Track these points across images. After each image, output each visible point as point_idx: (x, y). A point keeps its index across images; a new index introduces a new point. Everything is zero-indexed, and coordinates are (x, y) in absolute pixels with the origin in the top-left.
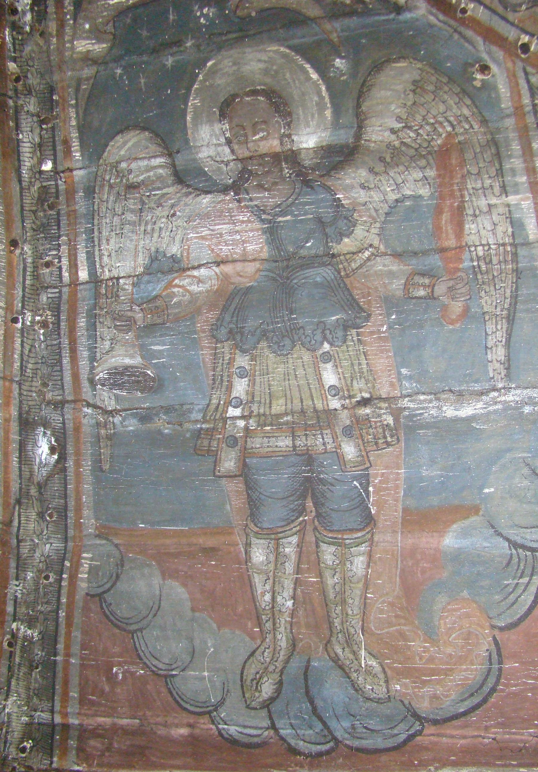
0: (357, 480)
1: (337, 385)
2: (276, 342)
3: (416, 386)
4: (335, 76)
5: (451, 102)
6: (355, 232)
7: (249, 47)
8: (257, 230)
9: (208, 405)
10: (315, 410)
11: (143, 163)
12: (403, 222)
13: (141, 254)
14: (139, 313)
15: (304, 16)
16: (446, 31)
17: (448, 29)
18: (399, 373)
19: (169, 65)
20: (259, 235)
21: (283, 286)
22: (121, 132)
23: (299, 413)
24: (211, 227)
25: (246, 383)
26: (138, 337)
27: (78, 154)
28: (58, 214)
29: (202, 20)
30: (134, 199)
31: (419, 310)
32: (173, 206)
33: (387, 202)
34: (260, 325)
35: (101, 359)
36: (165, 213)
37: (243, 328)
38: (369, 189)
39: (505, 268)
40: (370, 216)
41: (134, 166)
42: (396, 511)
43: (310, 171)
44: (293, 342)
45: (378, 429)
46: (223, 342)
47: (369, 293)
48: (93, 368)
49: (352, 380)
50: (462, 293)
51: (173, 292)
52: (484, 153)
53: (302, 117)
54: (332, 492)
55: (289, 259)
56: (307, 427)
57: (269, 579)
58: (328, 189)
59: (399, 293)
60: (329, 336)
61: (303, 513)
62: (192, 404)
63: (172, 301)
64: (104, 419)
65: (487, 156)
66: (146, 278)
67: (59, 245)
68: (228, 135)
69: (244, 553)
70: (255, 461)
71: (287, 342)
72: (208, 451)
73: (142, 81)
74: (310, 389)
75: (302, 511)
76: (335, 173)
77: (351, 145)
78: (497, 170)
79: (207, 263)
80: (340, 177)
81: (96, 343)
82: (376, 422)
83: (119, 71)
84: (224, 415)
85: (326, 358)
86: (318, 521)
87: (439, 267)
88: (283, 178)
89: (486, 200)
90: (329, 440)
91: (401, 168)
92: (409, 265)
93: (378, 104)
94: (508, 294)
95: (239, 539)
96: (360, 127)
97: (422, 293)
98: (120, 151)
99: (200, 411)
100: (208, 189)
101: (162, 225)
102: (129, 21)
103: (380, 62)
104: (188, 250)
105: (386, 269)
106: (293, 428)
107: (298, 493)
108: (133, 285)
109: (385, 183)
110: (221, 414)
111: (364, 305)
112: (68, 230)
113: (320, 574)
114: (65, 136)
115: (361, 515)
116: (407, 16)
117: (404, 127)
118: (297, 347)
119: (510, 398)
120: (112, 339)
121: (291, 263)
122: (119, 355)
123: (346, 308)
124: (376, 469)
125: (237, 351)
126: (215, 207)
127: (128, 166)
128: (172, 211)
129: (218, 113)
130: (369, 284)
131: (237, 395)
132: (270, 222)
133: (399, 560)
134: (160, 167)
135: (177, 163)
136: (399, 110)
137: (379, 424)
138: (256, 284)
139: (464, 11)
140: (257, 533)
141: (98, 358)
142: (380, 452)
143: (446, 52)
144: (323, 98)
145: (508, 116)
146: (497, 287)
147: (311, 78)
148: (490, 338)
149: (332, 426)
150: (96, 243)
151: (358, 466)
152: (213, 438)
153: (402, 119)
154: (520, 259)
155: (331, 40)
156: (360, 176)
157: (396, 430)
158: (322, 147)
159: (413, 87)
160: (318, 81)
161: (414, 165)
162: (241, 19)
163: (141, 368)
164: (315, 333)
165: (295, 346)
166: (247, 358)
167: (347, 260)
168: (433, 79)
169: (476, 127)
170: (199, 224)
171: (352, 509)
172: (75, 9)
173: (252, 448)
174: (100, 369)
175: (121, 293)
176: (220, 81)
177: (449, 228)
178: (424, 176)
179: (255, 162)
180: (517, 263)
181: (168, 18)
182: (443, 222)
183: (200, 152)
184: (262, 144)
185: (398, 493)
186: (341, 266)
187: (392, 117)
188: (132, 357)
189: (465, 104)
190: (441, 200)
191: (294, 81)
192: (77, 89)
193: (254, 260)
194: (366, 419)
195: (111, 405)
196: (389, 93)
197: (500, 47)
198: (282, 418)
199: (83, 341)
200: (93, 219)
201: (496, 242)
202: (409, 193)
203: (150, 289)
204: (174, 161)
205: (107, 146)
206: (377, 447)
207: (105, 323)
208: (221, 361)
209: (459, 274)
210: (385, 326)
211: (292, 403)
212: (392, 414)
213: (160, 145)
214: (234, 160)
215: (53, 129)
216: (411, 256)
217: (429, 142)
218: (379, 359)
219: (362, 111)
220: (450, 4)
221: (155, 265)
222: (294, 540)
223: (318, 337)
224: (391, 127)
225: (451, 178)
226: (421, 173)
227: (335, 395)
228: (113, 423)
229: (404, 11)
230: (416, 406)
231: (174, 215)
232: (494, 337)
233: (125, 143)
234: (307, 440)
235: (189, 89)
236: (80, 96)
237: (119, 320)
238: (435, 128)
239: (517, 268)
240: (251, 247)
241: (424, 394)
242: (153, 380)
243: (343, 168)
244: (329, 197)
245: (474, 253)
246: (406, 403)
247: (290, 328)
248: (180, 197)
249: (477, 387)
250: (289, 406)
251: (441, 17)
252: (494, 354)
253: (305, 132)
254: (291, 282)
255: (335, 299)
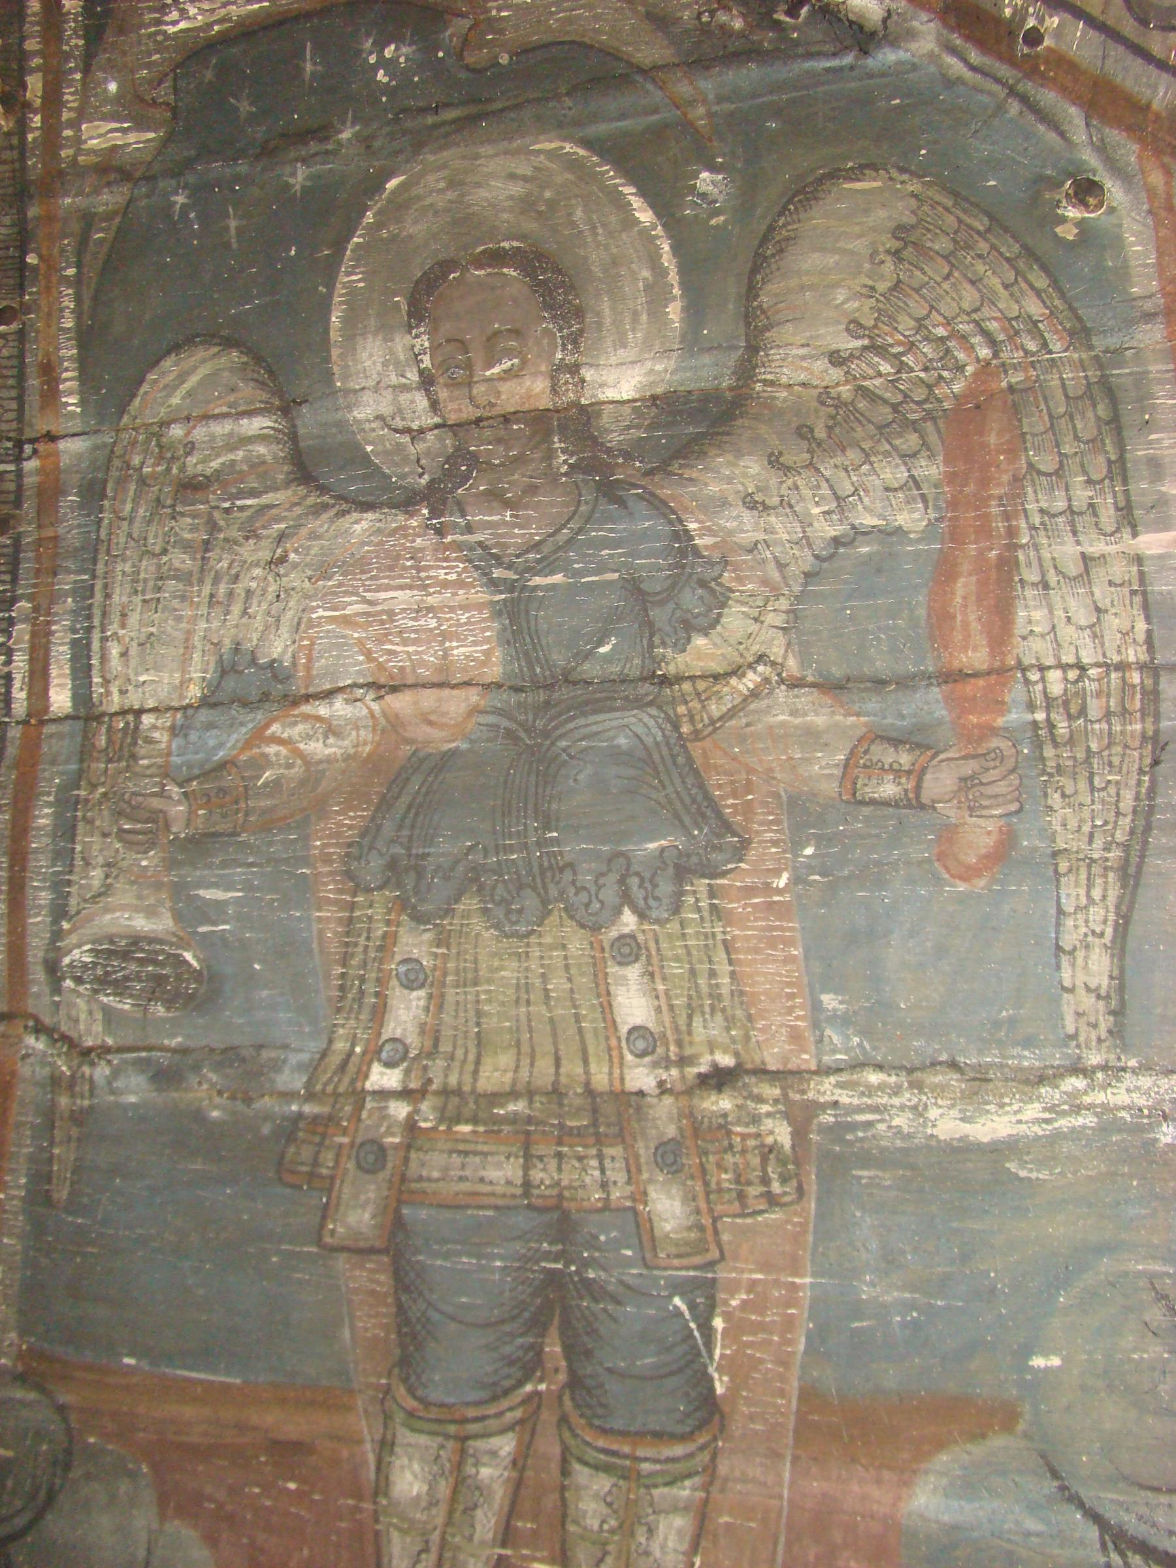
0: (682, 1295)
1: (650, 1025)
2: (503, 900)
3: (860, 1045)
4: (696, 216)
5: (995, 282)
6: (724, 620)
7: (490, 141)
8: (480, 607)
9: (324, 1054)
10: (590, 1092)
11: (221, 429)
12: (850, 597)
13: (197, 656)
14: (179, 802)
15: (630, 64)
16: (990, 93)
17: (996, 88)
18: (817, 1006)
19: (298, 187)
20: (484, 620)
21: (533, 754)
22: (176, 348)
23: (548, 1094)
24: (368, 595)
25: (422, 1003)
26: (171, 864)
27: (72, 400)
28: (17, 544)
29: (381, 76)
30: (194, 517)
31: (878, 836)
32: (281, 537)
33: (810, 545)
34: (467, 854)
35: (78, 913)
36: (265, 555)
37: (425, 856)
38: (766, 508)
39: (1123, 733)
40: (765, 582)
41: (199, 433)
42: (782, 1393)
43: (620, 460)
44: (545, 902)
45: (749, 1156)
46: (369, 890)
47: (749, 782)
48: (58, 935)
49: (690, 1017)
50: (996, 796)
51: (265, 756)
52: (1078, 417)
53: (608, 321)
54: (615, 1320)
55: (552, 685)
56: (565, 1135)
57: (426, 1550)
58: (660, 507)
59: (831, 788)
60: (638, 894)
61: (533, 1371)
62: (286, 1047)
63: (259, 777)
64: (70, 1068)
65: (1086, 426)
66: (204, 715)
67: (11, 622)
68: (426, 362)
69: (373, 1467)
70: (423, 1213)
71: (530, 901)
72: (312, 1176)
73: (233, 224)
74: (580, 1030)
75: (532, 1365)
76: (680, 467)
77: (729, 395)
78: (1109, 462)
79: (355, 685)
80: (694, 475)
81: (70, 872)
82: (744, 1137)
83: (180, 199)
84: (359, 1085)
85: (626, 950)
86: (573, 1399)
87: (940, 722)
88: (552, 477)
89: (1078, 543)
90: (616, 1173)
91: (853, 455)
92: (858, 715)
93: (802, 288)
94: (1127, 802)
95: (367, 1430)
96: (753, 349)
97: (889, 789)
98: (169, 396)
99: (300, 1067)
100: (369, 499)
101: (254, 585)
102: (209, 75)
103: (810, 179)
104: (311, 650)
105: (798, 721)
106: (528, 1133)
107: (527, 1315)
108: (173, 730)
109: (806, 492)
110: (353, 1081)
111: (735, 814)
112: (35, 586)
113: (564, 1552)
114: (47, 355)
115: (687, 1394)
116: (888, 56)
117: (865, 348)
118: (554, 918)
119: (1119, 1096)
120: (108, 865)
121: (556, 695)
122: (123, 908)
123: (687, 820)
124: (735, 1269)
125: (404, 917)
126: (381, 543)
127: (187, 434)
128: (279, 551)
129: (404, 307)
130: (752, 761)
131: (398, 1034)
132: (511, 586)
133: (782, 1539)
134: (261, 438)
135: (302, 431)
136: (856, 305)
137: (751, 1143)
138: (465, 746)
139: (1033, 38)
140: (411, 1414)
141: (73, 911)
142: (749, 1221)
143: (985, 149)
144: (664, 273)
145: (1149, 317)
146: (1097, 782)
147: (638, 222)
148: (1070, 922)
149: (628, 1138)
150: (96, 622)
151: (688, 1255)
152: (327, 1142)
153: (861, 326)
154: (1165, 706)
155: (691, 124)
156: (745, 475)
157: (797, 1163)
158: (654, 398)
159: (895, 244)
160: (655, 229)
161: (888, 447)
162: (474, 71)
163: (171, 944)
164: (601, 881)
165: (550, 912)
166: (427, 936)
167: (698, 694)
168: (950, 220)
169: (1056, 346)
170: (340, 585)
171: (662, 1377)
172: (87, 45)
173: (420, 1179)
174: (73, 939)
175: (142, 749)
176: (415, 228)
177: (972, 617)
178: (912, 477)
179: (488, 433)
180: (1157, 717)
181: (300, 70)
182: (959, 599)
183: (357, 404)
184: (505, 387)
185: (790, 1342)
186: (682, 709)
187: (838, 323)
188: (151, 912)
189: (1032, 287)
190: (953, 541)
191: (594, 228)
192: (83, 241)
193: (467, 684)
194: (720, 1127)
195: (93, 1034)
196: (832, 260)
197: (1130, 129)
198: (502, 1106)
199: (41, 864)
200: (95, 561)
201: (1101, 659)
202: (869, 521)
203: (212, 743)
204: (294, 426)
205: (141, 381)
206: (744, 1205)
207: (98, 823)
208: (362, 940)
209: (995, 743)
210: (785, 876)
211: (532, 1065)
212: (787, 1116)
213: (263, 384)
214: (437, 426)
215: (21, 334)
216: (866, 689)
217: (930, 387)
218: (765, 962)
219: (760, 307)
220: (998, 21)
221: (230, 684)
222: (506, 1445)
223: (610, 894)
224: (834, 347)
225: (985, 483)
226: (903, 468)
227: (641, 1055)
228: (91, 1080)
229: (879, 46)
230: (856, 1101)
231: (283, 560)
232: (1081, 923)
233: (182, 377)
234: (560, 1169)
235: (339, 245)
236: (87, 258)
237: (131, 819)
238: (948, 351)
239: (1157, 732)
240: (462, 650)
241: (880, 1067)
242: (197, 976)
243: (702, 454)
244: (663, 528)
245: (1039, 687)
246: (826, 1089)
247: (541, 866)
248: (299, 517)
249: (1029, 1059)
250: (524, 1074)
251: (974, 56)
252: (1078, 969)
253: (613, 360)
254: (553, 744)
255: (660, 796)
